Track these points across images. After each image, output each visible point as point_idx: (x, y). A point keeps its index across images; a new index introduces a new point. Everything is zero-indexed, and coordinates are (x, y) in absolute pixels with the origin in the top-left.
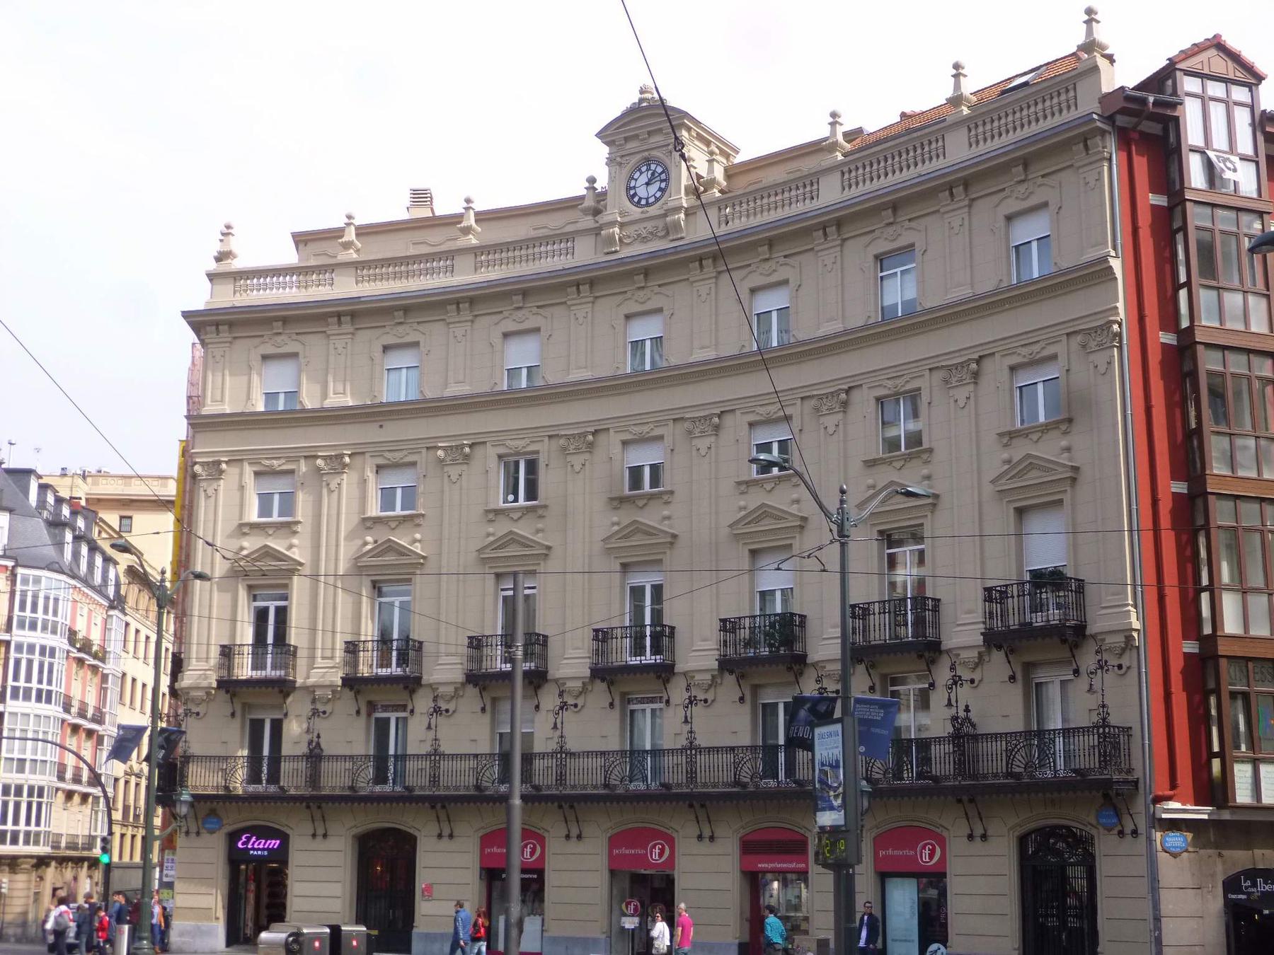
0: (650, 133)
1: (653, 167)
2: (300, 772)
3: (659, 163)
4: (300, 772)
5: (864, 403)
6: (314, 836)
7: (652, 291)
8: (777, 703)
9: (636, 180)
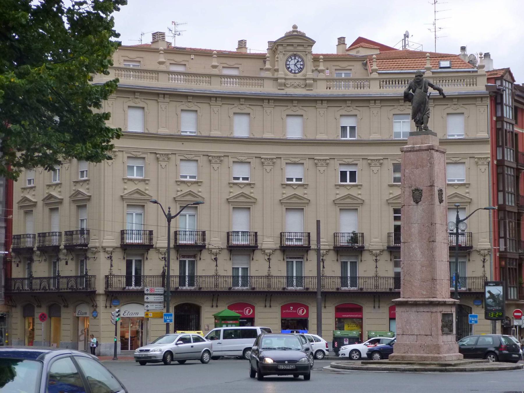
0: (298, 45)
1: (297, 58)
2: (281, 282)
3: (300, 57)
4: (281, 282)
5: (389, 165)
6: (212, 306)
7: (299, 108)
8: (347, 262)
9: (290, 62)
